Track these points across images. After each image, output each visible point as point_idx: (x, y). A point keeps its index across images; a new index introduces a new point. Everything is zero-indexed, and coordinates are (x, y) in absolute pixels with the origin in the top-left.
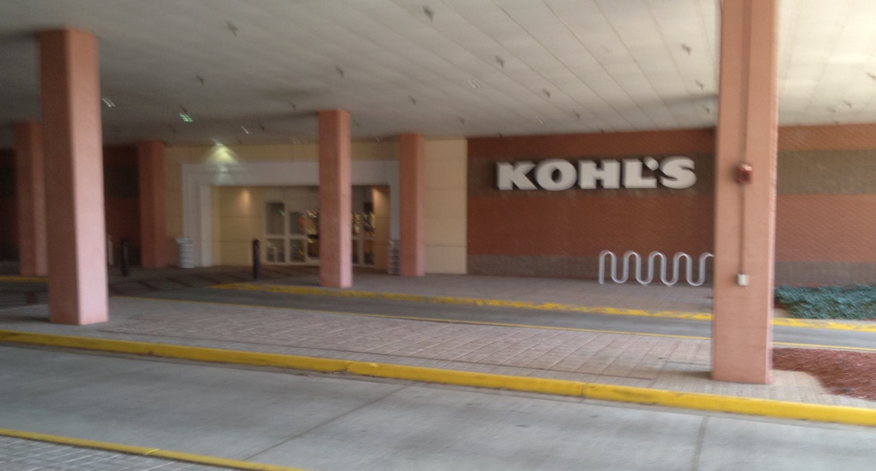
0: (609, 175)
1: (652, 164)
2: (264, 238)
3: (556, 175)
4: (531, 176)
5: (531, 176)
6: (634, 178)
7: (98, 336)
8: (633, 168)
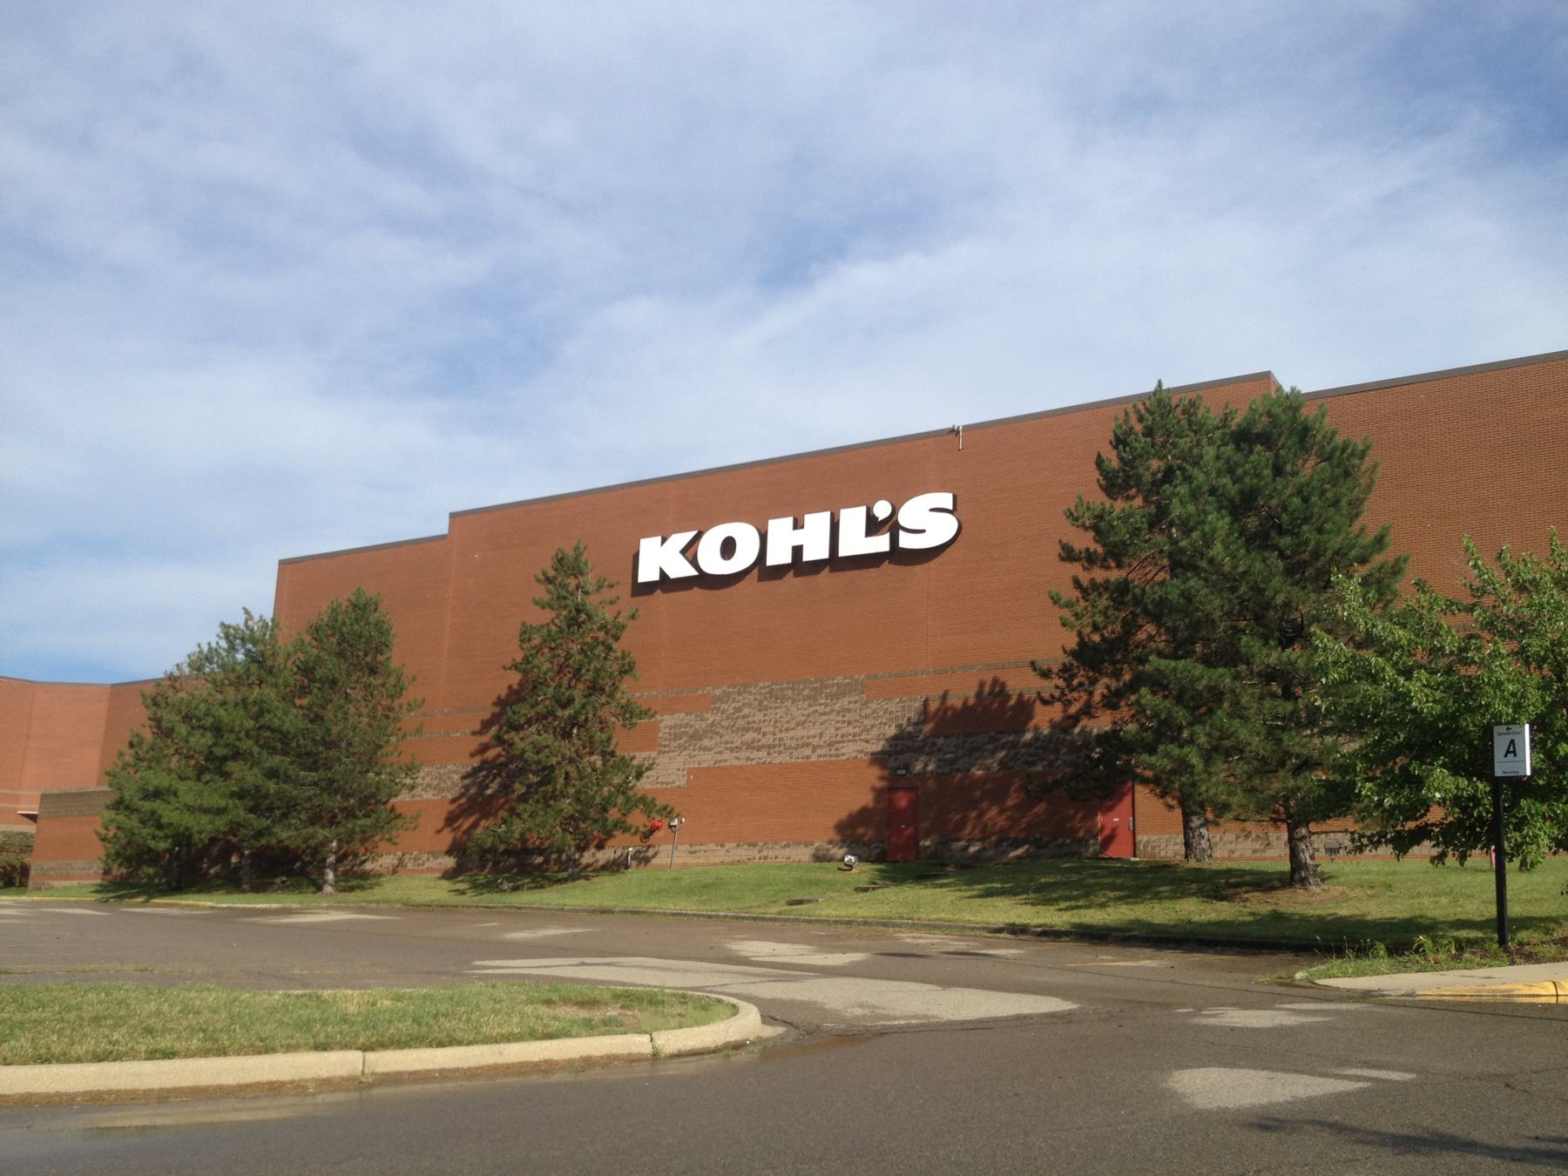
4: (690, 552)
5: (690, 552)
6: (856, 542)
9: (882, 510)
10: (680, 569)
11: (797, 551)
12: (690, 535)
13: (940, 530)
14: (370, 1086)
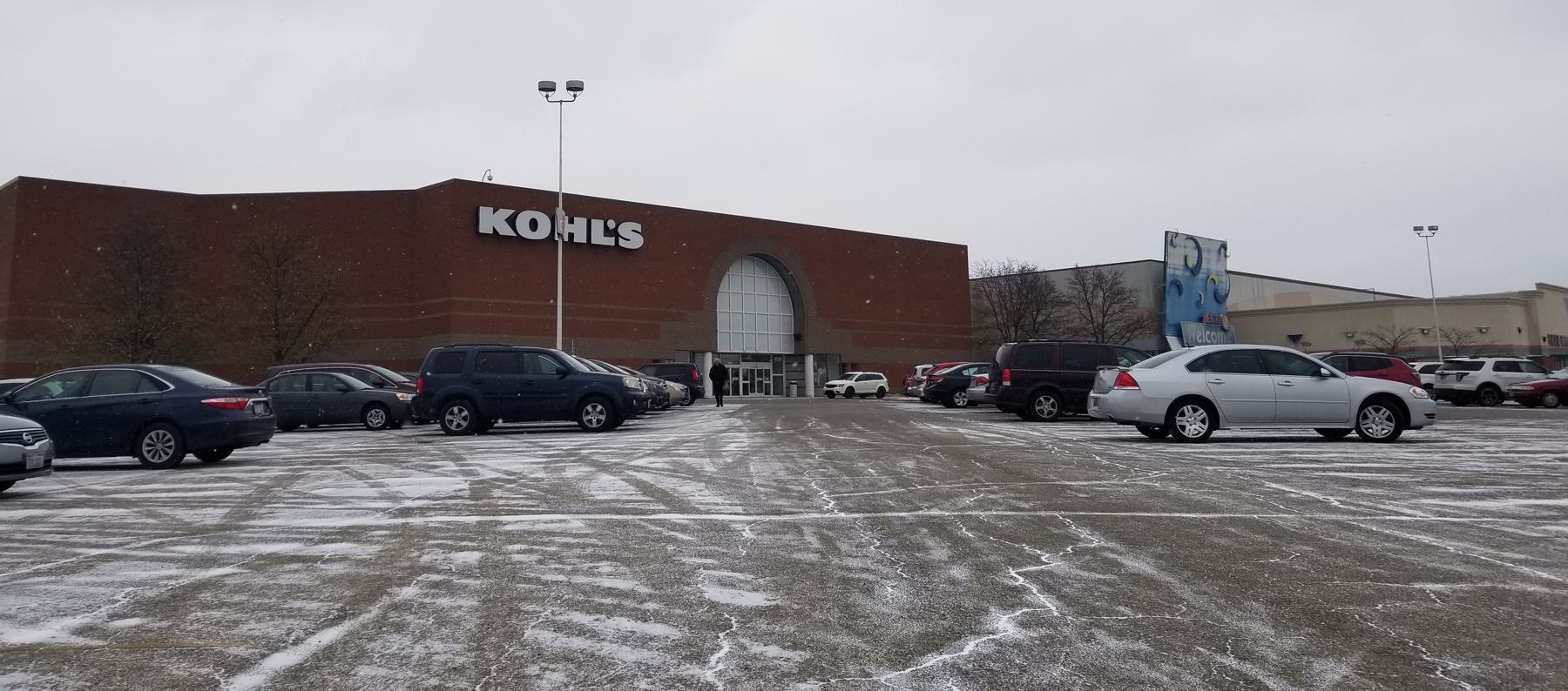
1: (611, 224)
4: (511, 221)
5: (511, 221)
6: (599, 238)
8: (597, 225)
9: (611, 224)
10: (505, 230)
13: (636, 242)
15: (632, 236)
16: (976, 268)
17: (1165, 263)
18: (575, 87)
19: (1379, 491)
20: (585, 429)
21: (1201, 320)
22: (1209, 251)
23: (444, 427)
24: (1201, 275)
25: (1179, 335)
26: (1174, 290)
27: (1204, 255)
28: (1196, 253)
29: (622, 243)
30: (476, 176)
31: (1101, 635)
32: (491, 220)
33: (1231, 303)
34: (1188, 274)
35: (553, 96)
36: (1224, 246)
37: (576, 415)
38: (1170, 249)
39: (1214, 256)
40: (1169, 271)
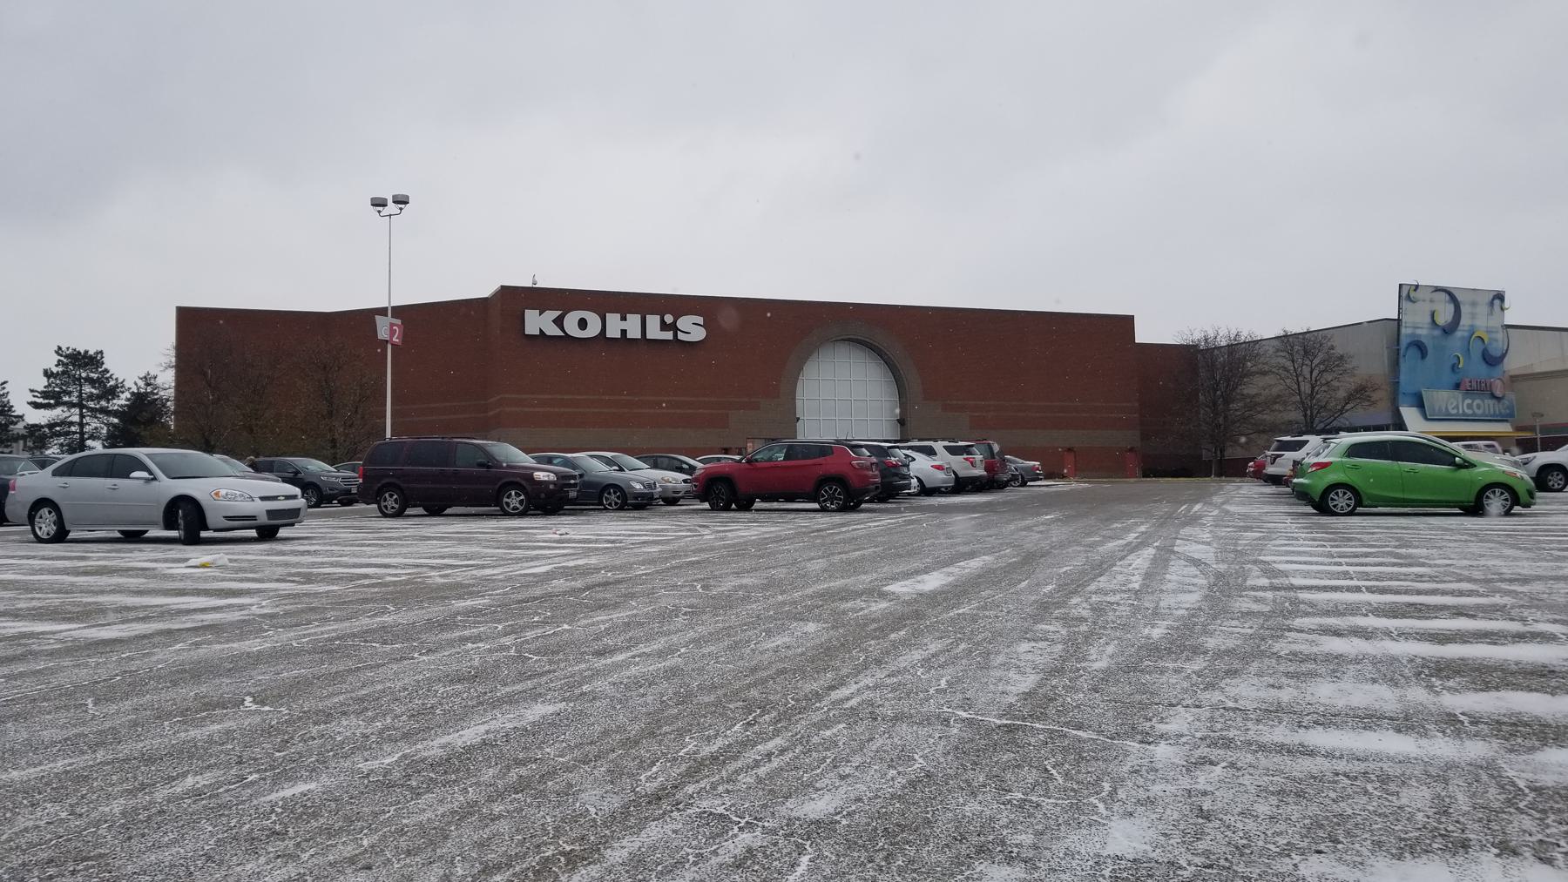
0: (633, 326)
1: (669, 319)
2: (20, 425)
3: (583, 324)
4: (559, 321)
5: (559, 321)
6: (655, 332)
7: (1124, 507)
8: (653, 321)
9: (669, 319)
10: (553, 331)
11: (624, 332)
12: (559, 313)
13: (698, 334)
14: (1513, 673)
15: (692, 329)
16: (1142, 336)
17: (1399, 320)
18: (401, 201)
19: (208, 586)
20: (506, 514)
21: (1457, 386)
22: (1474, 304)
23: (502, 509)
24: (1460, 333)
25: (1420, 404)
26: (1414, 352)
27: (1465, 310)
28: (1451, 308)
29: (681, 336)
30: (526, 283)
31: (611, 691)
32: (537, 322)
33: (1513, 364)
34: (1437, 332)
35: (386, 211)
36: (1500, 297)
37: (498, 503)
38: (1406, 304)
39: (1483, 309)
40: (1403, 331)
